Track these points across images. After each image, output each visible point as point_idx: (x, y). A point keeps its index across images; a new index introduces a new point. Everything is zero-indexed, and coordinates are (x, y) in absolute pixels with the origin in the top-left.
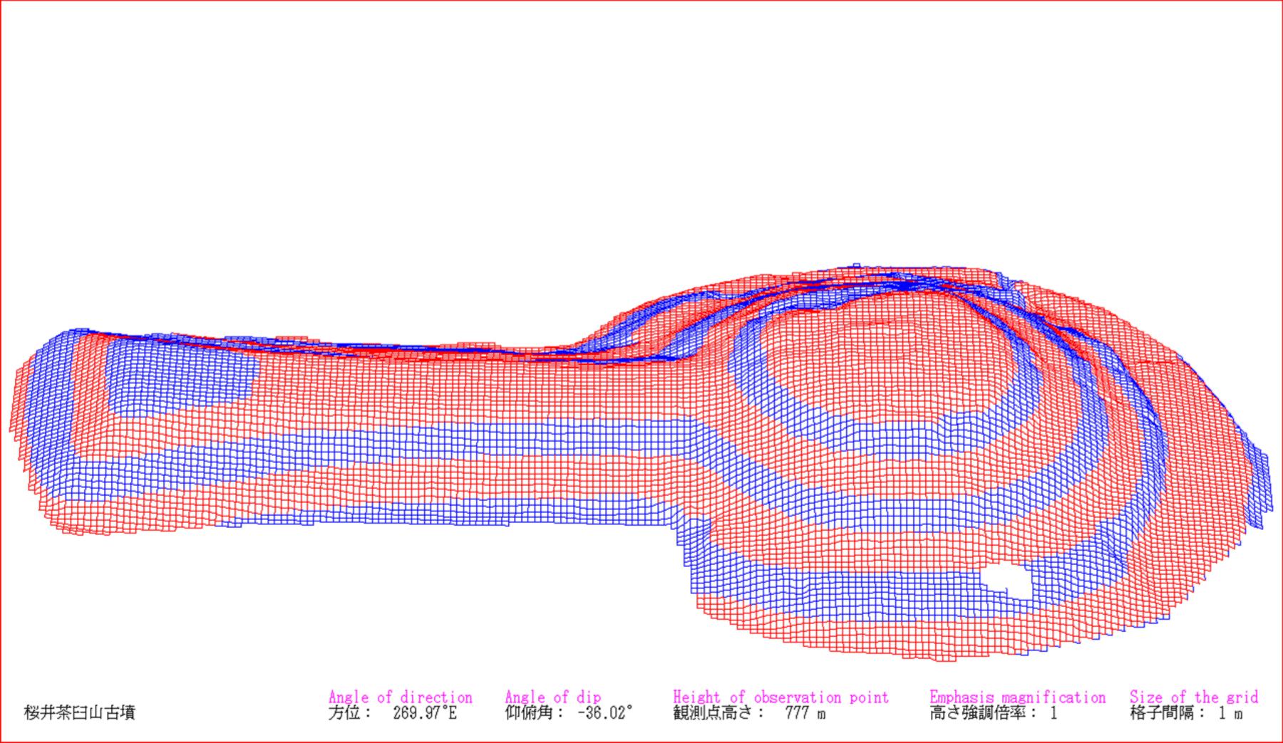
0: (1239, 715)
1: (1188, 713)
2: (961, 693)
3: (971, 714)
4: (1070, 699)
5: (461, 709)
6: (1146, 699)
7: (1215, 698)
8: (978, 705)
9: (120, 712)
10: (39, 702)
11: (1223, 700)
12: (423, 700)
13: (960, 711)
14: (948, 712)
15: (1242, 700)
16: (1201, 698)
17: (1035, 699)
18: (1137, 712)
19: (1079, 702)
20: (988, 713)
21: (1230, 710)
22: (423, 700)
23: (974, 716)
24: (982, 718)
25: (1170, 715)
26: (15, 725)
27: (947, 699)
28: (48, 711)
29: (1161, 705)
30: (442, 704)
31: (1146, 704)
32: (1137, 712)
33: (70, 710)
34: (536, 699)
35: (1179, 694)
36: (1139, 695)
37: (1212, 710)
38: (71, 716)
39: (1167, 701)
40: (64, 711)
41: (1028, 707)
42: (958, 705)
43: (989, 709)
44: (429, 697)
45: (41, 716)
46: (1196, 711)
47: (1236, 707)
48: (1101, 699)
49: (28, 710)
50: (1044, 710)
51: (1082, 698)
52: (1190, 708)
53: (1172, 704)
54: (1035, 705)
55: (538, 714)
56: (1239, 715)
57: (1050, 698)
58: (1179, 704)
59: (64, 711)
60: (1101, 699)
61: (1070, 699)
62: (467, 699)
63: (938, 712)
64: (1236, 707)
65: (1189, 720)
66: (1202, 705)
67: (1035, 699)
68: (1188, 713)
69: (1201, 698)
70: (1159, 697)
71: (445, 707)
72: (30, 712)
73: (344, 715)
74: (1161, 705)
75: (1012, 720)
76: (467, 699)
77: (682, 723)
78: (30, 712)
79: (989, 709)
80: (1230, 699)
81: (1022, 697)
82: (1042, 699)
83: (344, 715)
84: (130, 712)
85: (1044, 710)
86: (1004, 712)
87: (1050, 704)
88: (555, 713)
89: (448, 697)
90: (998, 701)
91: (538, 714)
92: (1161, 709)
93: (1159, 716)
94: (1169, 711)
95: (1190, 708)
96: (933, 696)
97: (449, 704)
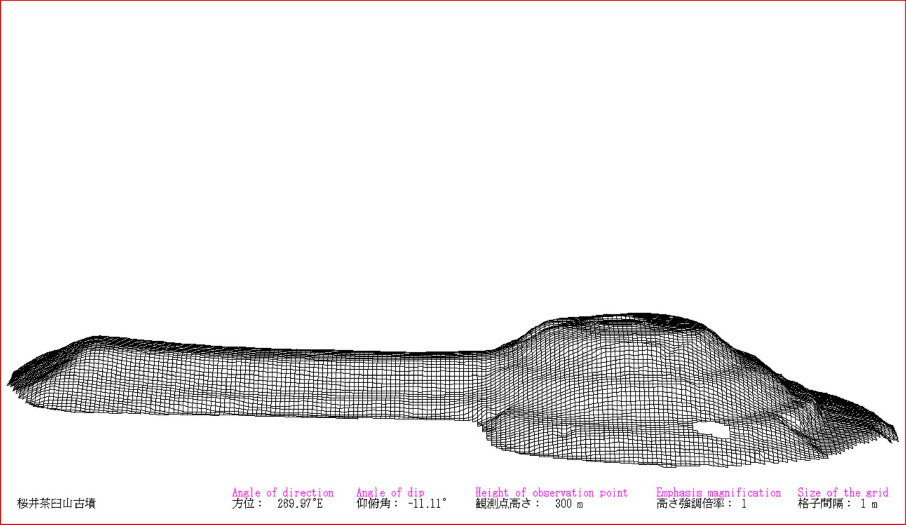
0: (875, 505)
1: (839, 504)
2: (678, 489)
3: (686, 504)
4: (756, 494)
5: (326, 501)
6: (809, 494)
7: (858, 493)
8: (691, 498)
9: (85, 503)
10: (28, 496)
11: (863, 495)
12: (299, 494)
13: (678, 503)
14: (669, 503)
15: (877, 495)
16: (848, 493)
17: (731, 494)
18: (803, 503)
19: (762, 496)
20: (697, 504)
21: (868, 502)
22: (299, 494)
23: (688, 506)
24: (693, 507)
25: (826, 505)
26: (11, 512)
27: (669, 494)
28: (34, 502)
29: (820, 498)
30: (312, 498)
31: (809, 498)
32: (803, 503)
33: (50, 502)
34: (378, 494)
35: (832, 490)
36: (804, 491)
37: (856, 502)
38: (50, 506)
39: (824, 495)
40: (45, 502)
41: (726, 500)
42: (676, 498)
43: (699, 501)
44: (303, 493)
45: (29, 506)
46: (844, 502)
47: (873, 500)
48: (777, 494)
49: (19, 502)
50: (737, 502)
51: (764, 493)
52: (840, 500)
53: (827, 497)
54: (731, 498)
55: (380, 504)
56: (875, 505)
57: (742, 494)
58: (833, 497)
59: (45, 502)
60: (777, 494)
61: (756, 494)
62: (330, 494)
63: (662, 503)
64: (873, 500)
65: (839, 509)
66: (849, 498)
67: (731, 494)
68: (839, 504)
69: (848, 493)
70: (818, 493)
71: (314, 499)
72: (22, 503)
73: (243, 505)
74: (820, 498)
75: (715, 509)
76: (330, 494)
77: (482, 511)
78: (22, 503)
79: (699, 501)
80: (869, 494)
81: (722, 492)
82: (736, 494)
83: (243, 505)
84: (91, 503)
85: (737, 502)
86: (709, 503)
87: (742, 497)
88: (392, 504)
89: (317, 493)
90: (705, 496)
91: (380, 504)
92: (820, 501)
93: (818, 506)
94: (826, 502)
95: (840, 500)
96: (659, 492)
97: (317, 497)
